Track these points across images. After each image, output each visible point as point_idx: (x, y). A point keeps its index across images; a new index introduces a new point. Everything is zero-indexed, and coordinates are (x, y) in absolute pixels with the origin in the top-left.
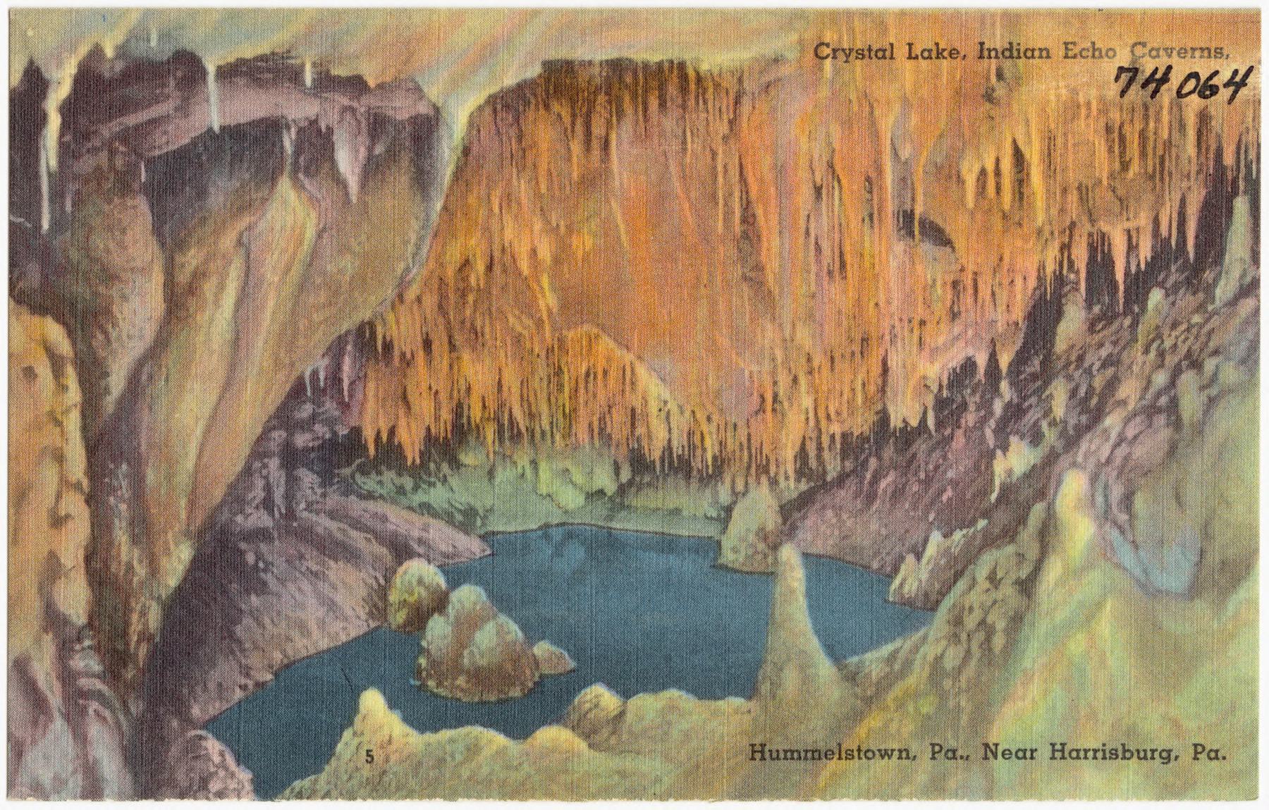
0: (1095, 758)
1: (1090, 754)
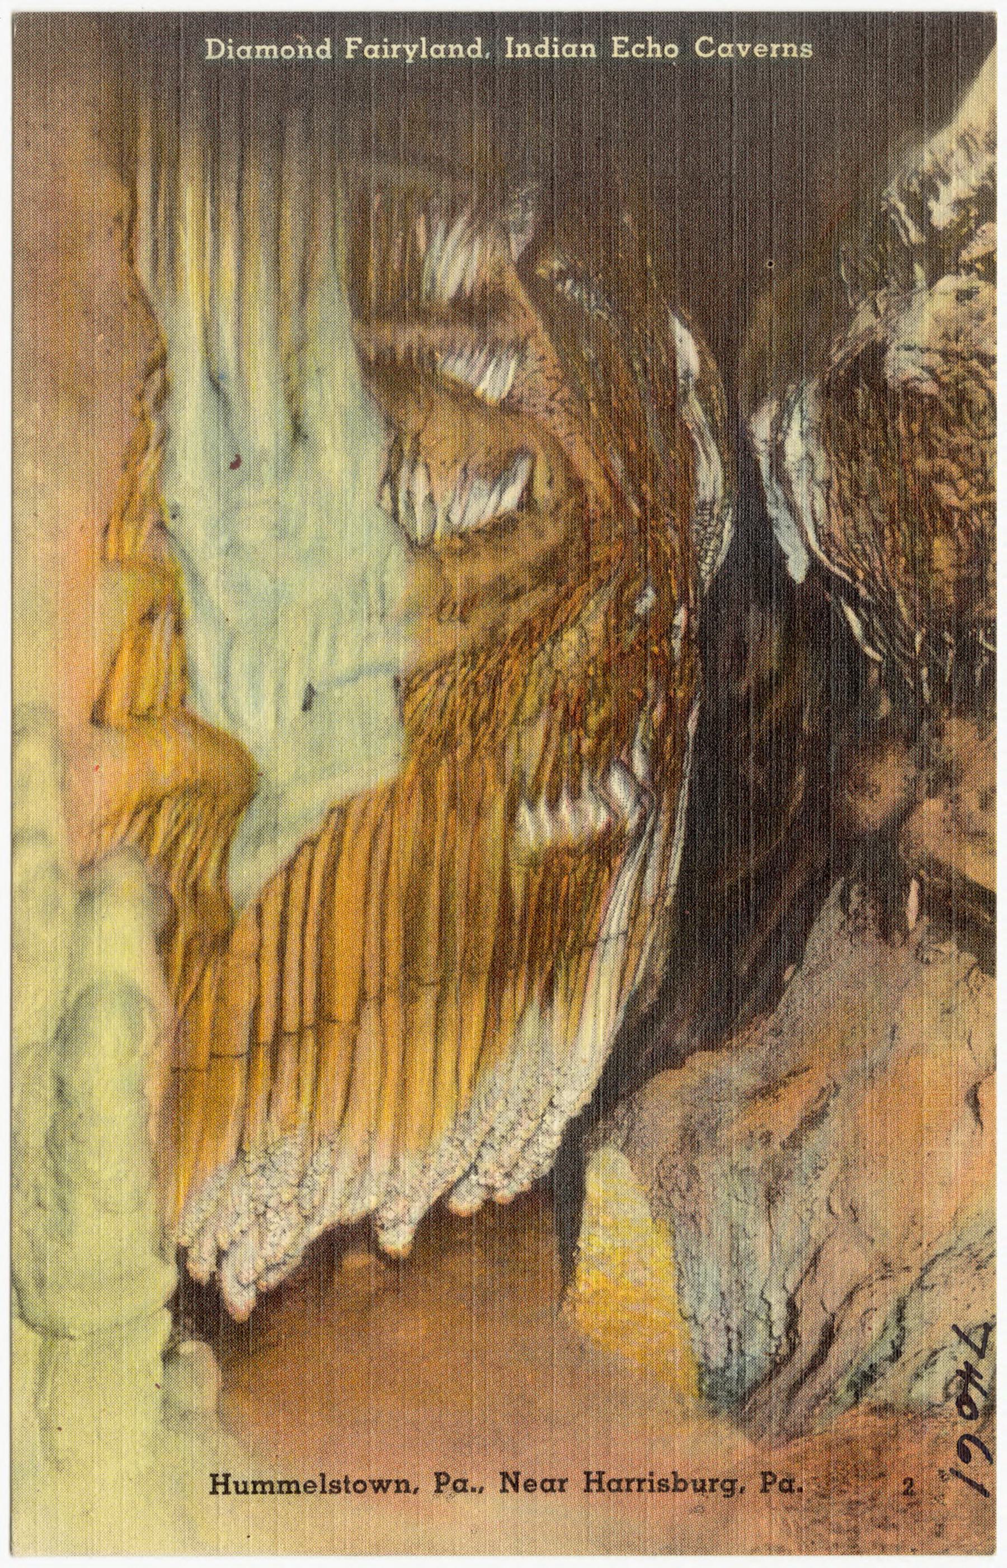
0: (640, 1490)
1: (634, 1485)
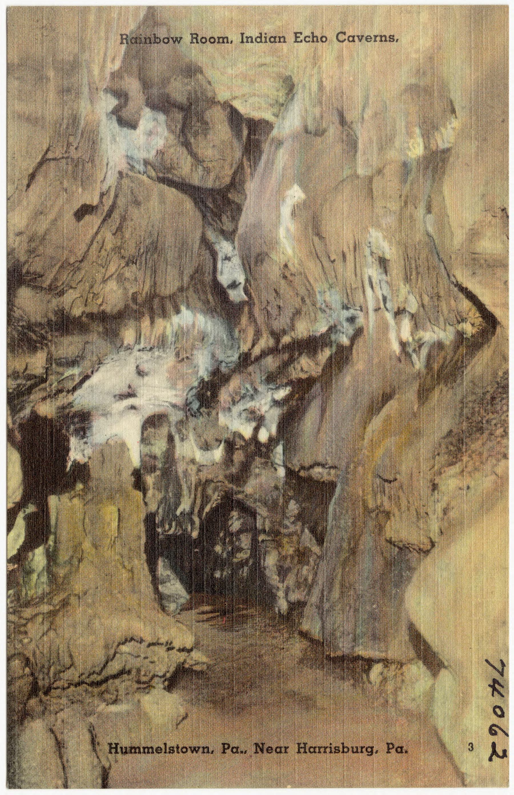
1: (322, 750)
